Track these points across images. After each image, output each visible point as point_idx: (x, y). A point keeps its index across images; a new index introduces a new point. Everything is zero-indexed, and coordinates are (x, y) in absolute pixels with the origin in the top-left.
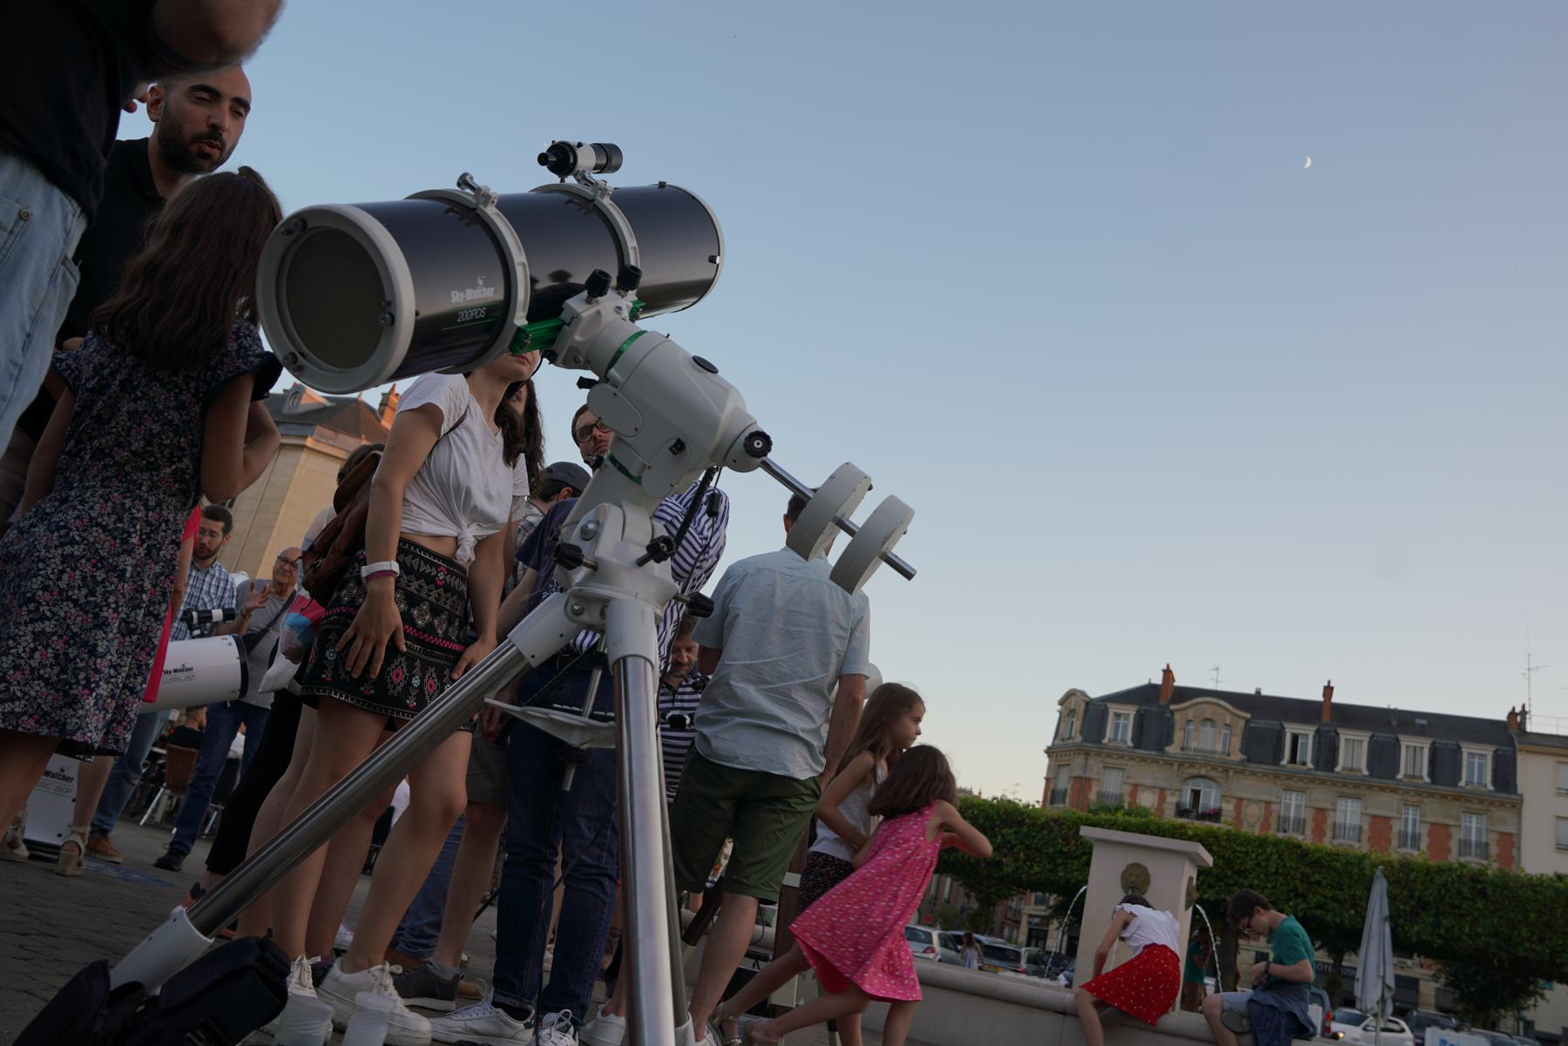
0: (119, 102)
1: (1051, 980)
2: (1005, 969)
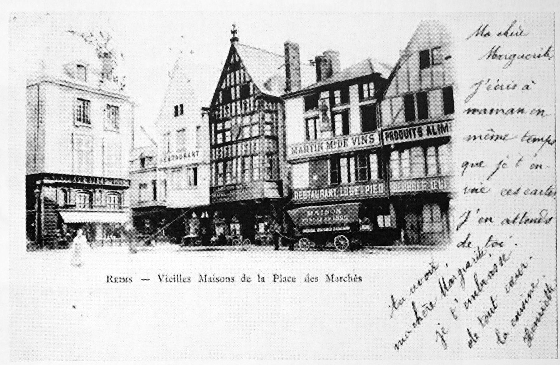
0: (366, 232)
1: (362, 106)
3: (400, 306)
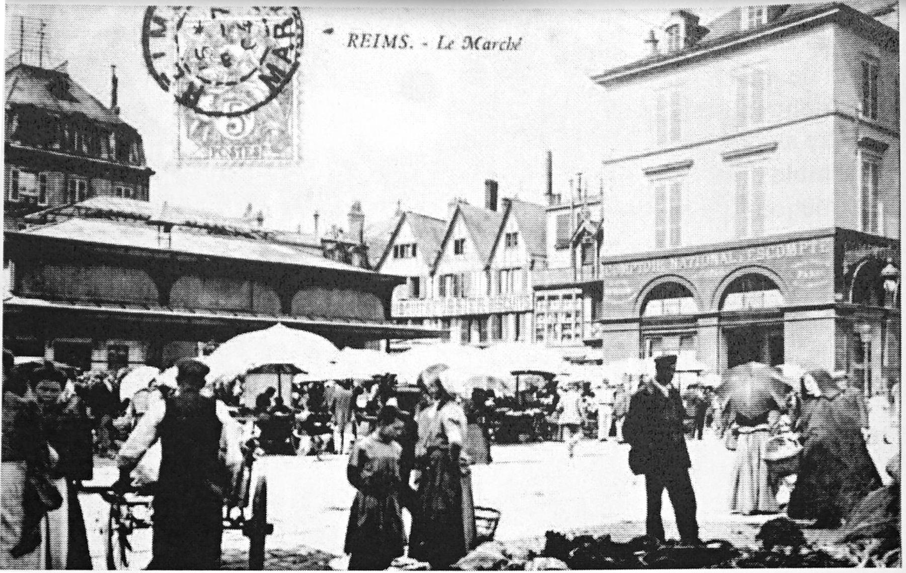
0: (318, 421)
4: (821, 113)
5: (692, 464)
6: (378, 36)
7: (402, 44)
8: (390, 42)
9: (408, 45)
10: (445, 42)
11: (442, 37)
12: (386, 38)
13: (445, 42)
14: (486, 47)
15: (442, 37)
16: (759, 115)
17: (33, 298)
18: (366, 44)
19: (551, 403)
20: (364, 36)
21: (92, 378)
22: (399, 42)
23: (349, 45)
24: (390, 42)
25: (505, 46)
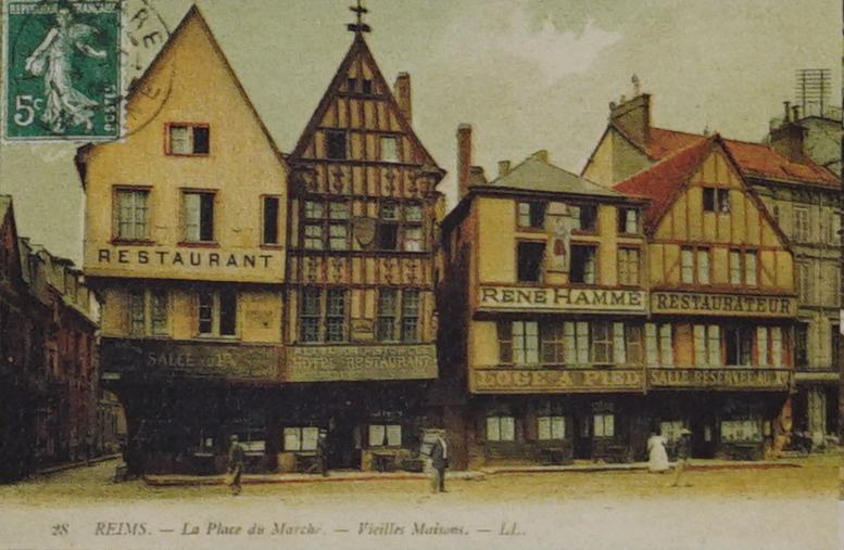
2: (598, 266)
3: (342, 179)
4: (251, 115)
5: (652, 454)
6: (121, 524)
7: (141, 531)
8: (132, 529)
9: (148, 531)
10: (189, 529)
11: (186, 525)
12: (128, 525)
13: (189, 529)
14: (290, 531)
15: (186, 525)
16: (625, 375)
17: (371, 56)
18: (111, 532)
19: (287, 430)
20: (110, 524)
21: (822, 221)
22: (139, 529)
23: (97, 534)
24: (132, 529)
25: (305, 531)
